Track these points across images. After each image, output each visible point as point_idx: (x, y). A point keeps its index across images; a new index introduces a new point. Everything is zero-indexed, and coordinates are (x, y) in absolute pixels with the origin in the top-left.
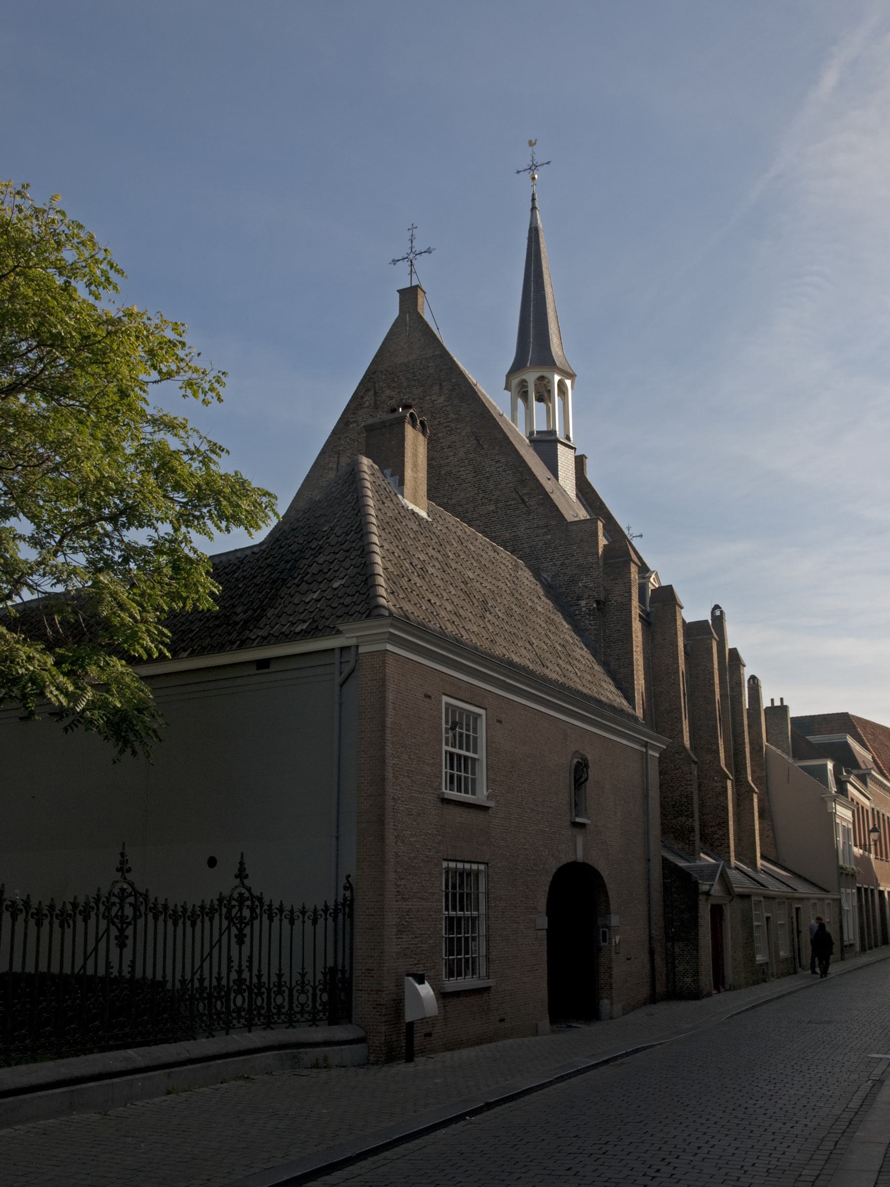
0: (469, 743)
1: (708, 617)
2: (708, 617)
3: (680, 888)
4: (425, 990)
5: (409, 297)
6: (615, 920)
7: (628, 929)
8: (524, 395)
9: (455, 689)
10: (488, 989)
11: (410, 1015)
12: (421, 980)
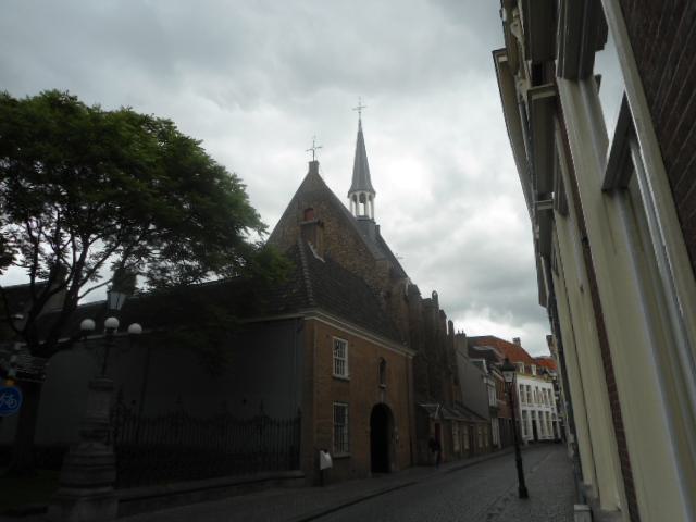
0: (341, 354)
1: (431, 297)
2: (431, 297)
3: (422, 415)
4: (328, 456)
5: (314, 166)
6: (396, 429)
7: (401, 433)
8: (355, 200)
9: (337, 333)
10: (349, 457)
11: (323, 467)
12: (326, 452)
